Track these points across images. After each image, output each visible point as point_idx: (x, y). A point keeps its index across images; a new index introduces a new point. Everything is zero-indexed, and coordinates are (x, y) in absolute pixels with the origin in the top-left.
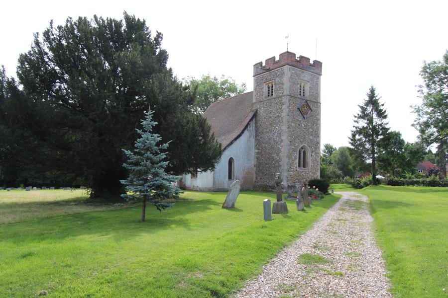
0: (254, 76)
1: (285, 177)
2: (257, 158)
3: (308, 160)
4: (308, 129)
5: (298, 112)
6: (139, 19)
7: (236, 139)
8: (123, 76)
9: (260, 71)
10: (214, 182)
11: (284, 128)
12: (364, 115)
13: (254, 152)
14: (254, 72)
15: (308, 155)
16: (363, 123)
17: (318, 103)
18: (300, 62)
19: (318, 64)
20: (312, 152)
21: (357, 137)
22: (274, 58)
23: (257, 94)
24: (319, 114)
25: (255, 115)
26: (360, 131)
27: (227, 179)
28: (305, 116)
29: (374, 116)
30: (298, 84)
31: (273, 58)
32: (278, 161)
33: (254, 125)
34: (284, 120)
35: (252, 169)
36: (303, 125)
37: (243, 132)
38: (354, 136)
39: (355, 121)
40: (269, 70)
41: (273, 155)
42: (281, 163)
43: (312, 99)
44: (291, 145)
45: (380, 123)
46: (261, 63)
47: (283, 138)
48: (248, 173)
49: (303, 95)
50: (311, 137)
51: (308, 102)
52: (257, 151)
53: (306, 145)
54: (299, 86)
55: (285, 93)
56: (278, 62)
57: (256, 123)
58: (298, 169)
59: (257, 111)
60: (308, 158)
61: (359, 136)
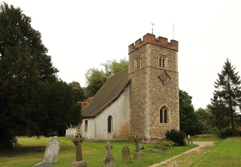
0: (129, 54)
1: (148, 131)
2: (131, 116)
3: (169, 117)
4: (168, 93)
5: (159, 80)
6: (12, 6)
7: (113, 101)
8: (236, 80)
9: (132, 50)
10: (96, 135)
11: (147, 92)
12: (222, 82)
13: (129, 111)
14: (129, 52)
15: (169, 113)
16: (221, 89)
17: (176, 73)
18: (159, 42)
19: (175, 43)
20: (172, 111)
21: (218, 99)
22: (140, 39)
23: (131, 67)
24: (177, 81)
25: (129, 83)
26: (219, 94)
27: (107, 132)
28: (165, 83)
29: (231, 83)
30: (158, 58)
31: (139, 39)
32: (144, 118)
33: (129, 91)
34: (147, 86)
35: (127, 124)
36: (163, 90)
37: (119, 96)
38: (216, 98)
39: (216, 87)
40: (137, 49)
41: (140, 113)
42: (145, 120)
43: (171, 70)
44: (153, 105)
45: (235, 87)
46: (133, 44)
47: (147, 99)
48: (125, 127)
49: (163, 67)
50: (171, 99)
51: (167, 72)
52: (131, 110)
53: (166, 105)
54: (159, 60)
55: (147, 65)
56: (142, 42)
57: (130, 89)
58: (160, 124)
59: (130, 80)
60: (169, 115)
61: (220, 98)
